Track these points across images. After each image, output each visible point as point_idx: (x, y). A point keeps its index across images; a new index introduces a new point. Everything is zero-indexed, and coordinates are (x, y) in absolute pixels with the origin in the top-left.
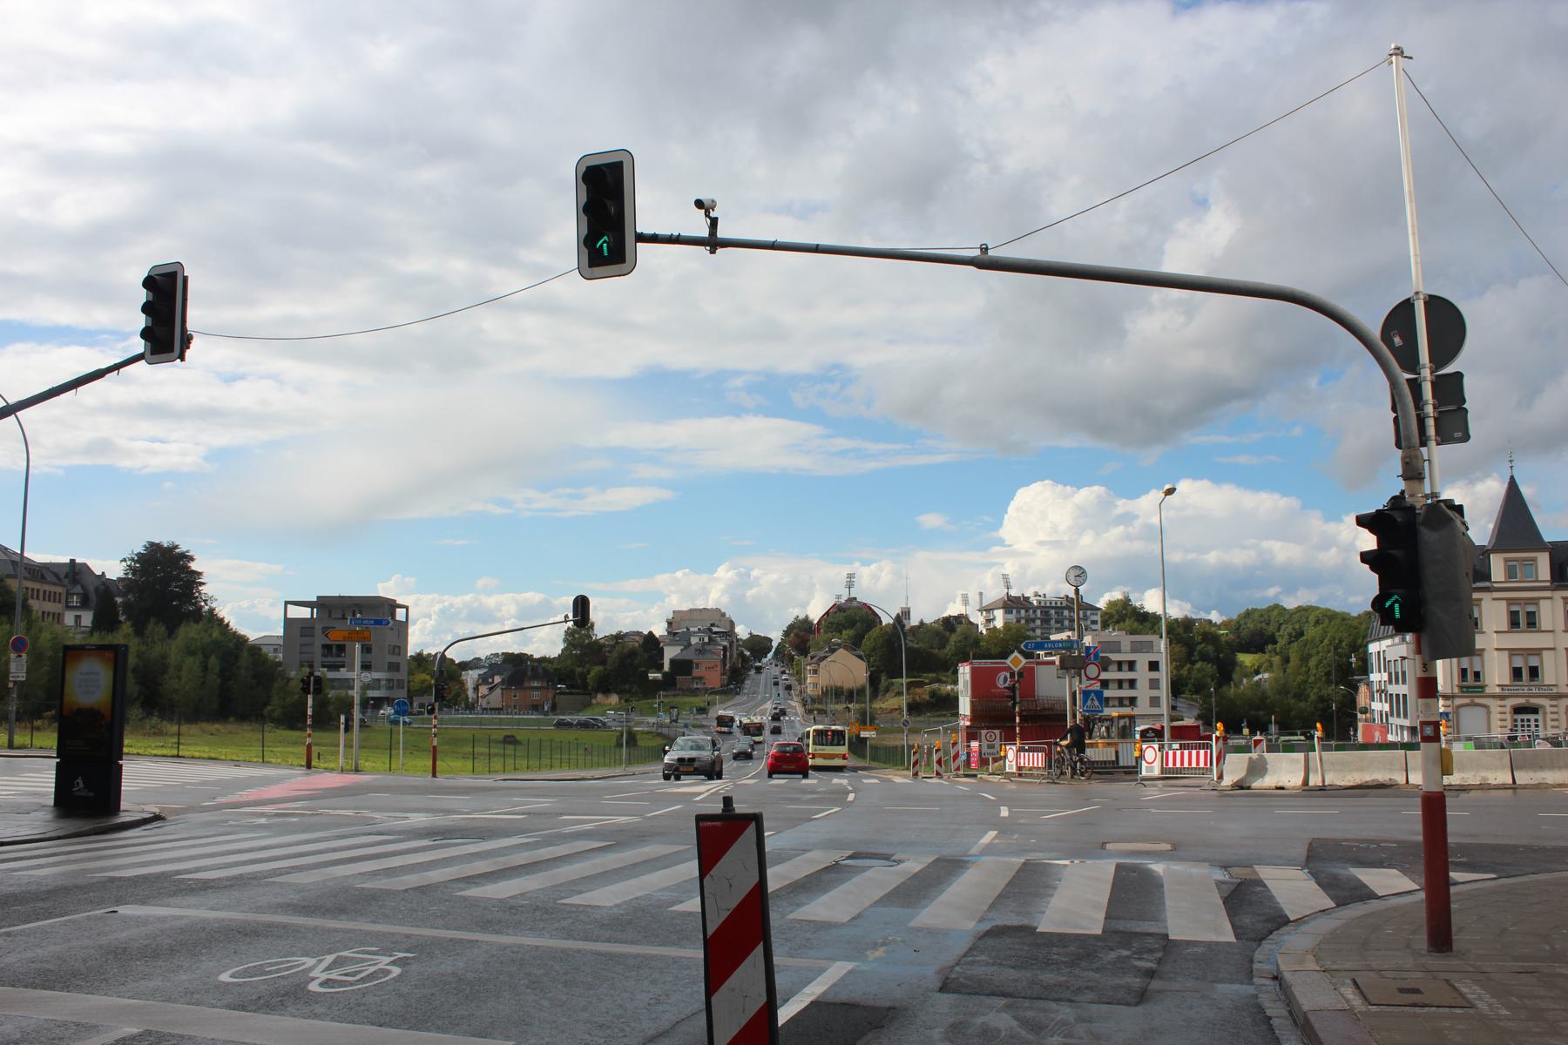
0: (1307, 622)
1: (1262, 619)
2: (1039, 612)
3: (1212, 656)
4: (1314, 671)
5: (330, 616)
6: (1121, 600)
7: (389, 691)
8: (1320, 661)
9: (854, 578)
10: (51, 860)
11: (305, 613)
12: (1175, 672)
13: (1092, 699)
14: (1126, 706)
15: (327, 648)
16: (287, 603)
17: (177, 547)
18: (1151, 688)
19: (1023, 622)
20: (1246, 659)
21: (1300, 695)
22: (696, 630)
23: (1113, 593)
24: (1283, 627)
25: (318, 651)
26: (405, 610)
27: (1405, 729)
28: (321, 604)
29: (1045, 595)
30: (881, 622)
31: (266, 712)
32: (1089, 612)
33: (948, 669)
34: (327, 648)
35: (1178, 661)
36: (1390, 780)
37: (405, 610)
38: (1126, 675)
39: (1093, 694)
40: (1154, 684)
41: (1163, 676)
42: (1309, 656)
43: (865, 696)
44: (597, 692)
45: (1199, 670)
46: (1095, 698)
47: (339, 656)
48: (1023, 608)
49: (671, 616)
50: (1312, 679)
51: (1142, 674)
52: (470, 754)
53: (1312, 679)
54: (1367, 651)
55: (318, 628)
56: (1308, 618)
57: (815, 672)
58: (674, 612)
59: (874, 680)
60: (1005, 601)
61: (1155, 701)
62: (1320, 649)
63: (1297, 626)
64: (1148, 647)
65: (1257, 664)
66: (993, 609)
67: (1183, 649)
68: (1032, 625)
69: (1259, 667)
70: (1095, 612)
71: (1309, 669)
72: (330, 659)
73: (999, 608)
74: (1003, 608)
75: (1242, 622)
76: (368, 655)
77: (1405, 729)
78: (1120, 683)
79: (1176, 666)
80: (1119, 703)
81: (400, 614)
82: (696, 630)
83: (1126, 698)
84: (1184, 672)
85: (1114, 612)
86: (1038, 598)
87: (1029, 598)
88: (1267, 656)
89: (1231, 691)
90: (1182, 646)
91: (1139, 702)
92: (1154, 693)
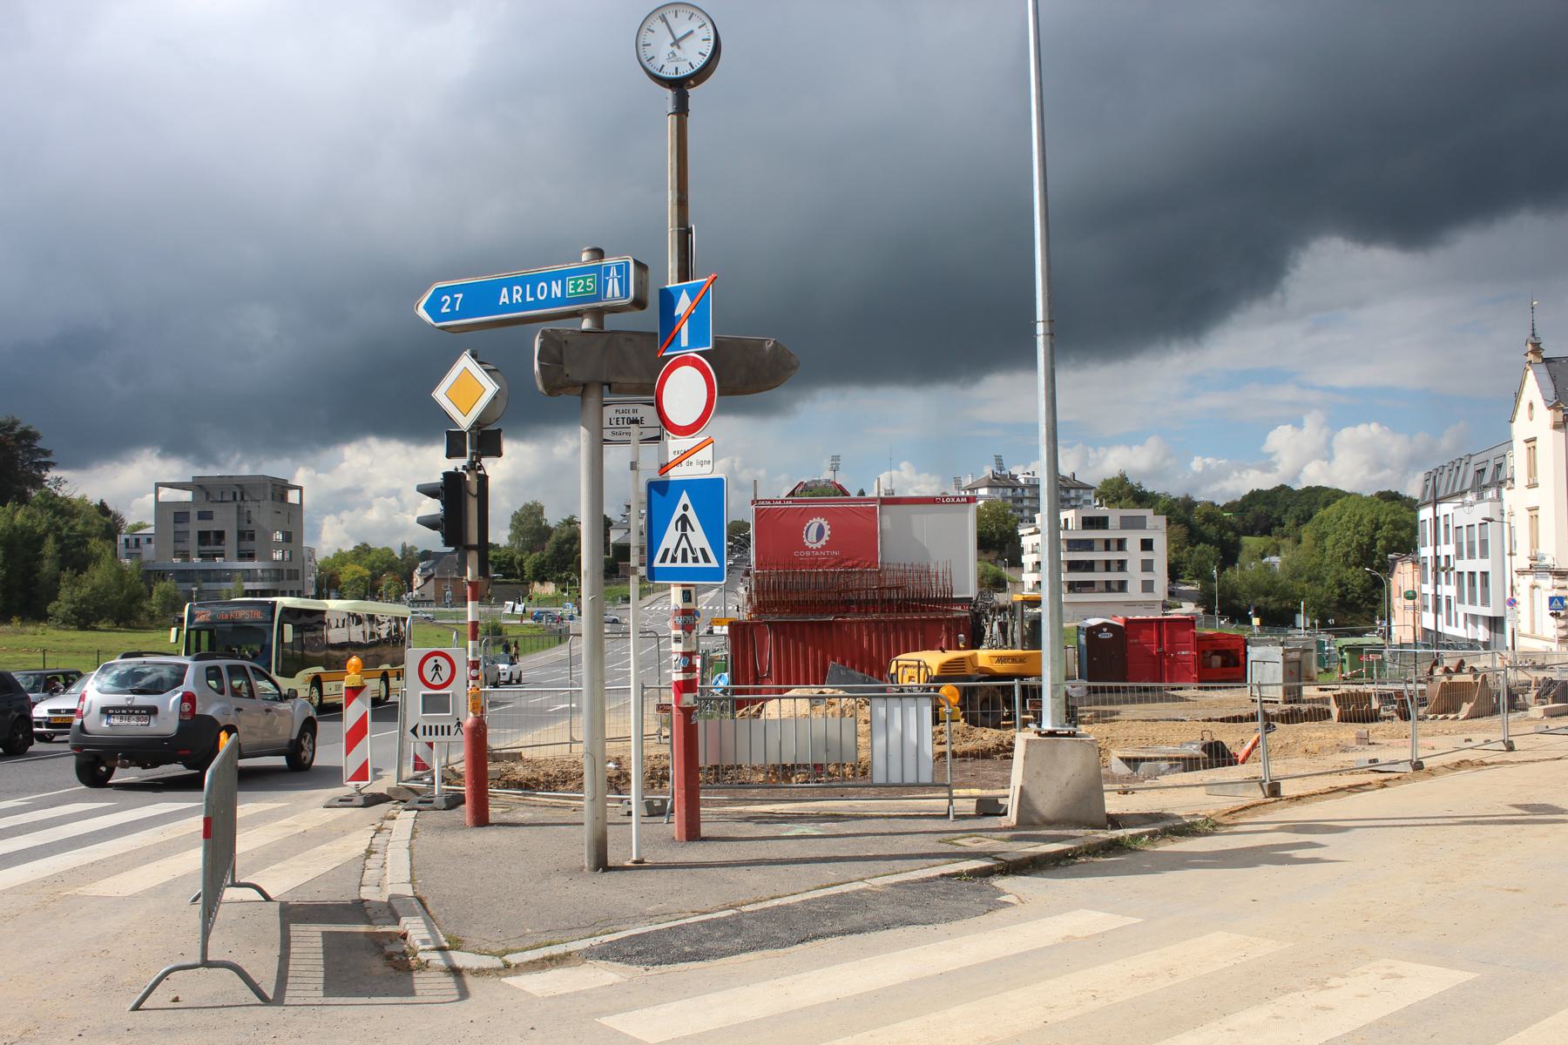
0: (1316, 503)
1: (1268, 501)
2: (1027, 490)
3: (1214, 538)
4: (1330, 552)
5: (207, 499)
6: (1117, 478)
7: (277, 583)
8: (1337, 541)
11: (186, 496)
12: (1174, 555)
13: (684, 520)
14: (1114, 591)
15: (204, 537)
16: (158, 485)
17: (15, 423)
18: (1144, 570)
19: (1010, 501)
20: (1251, 543)
21: (1316, 579)
23: (1042, 336)
24: (1290, 509)
26: (298, 491)
27: (1480, 620)
29: (1033, 473)
31: (50, 609)
32: (1081, 491)
34: (204, 537)
35: (1175, 545)
37: (298, 491)
38: (1114, 556)
39: (685, 499)
40: (1147, 566)
41: (1160, 556)
42: (1324, 535)
43: (1219, 597)
44: (533, 581)
45: (1199, 552)
46: (691, 515)
47: (218, 544)
48: (1010, 487)
50: (1327, 560)
51: (1134, 554)
53: (1327, 560)
54: (1416, 518)
55: (194, 513)
56: (1316, 499)
60: (990, 480)
61: (1148, 586)
62: (1337, 527)
63: (1306, 508)
64: (1139, 523)
65: (1262, 548)
66: (977, 488)
67: (1184, 529)
68: (1019, 505)
69: (1265, 551)
70: (1088, 491)
71: (1325, 550)
72: (207, 548)
73: (984, 487)
74: (988, 487)
75: (1246, 504)
77: (1480, 620)
78: (1108, 565)
79: (1176, 548)
80: (1119, 587)
81: (293, 497)
84: (1184, 554)
85: (1109, 492)
86: (1026, 476)
87: (1017, 476)
88: (1273, 539)
89: (1234, 575)
90: (1182, 527)
91: (1129, 587)
92: (1147, 576)
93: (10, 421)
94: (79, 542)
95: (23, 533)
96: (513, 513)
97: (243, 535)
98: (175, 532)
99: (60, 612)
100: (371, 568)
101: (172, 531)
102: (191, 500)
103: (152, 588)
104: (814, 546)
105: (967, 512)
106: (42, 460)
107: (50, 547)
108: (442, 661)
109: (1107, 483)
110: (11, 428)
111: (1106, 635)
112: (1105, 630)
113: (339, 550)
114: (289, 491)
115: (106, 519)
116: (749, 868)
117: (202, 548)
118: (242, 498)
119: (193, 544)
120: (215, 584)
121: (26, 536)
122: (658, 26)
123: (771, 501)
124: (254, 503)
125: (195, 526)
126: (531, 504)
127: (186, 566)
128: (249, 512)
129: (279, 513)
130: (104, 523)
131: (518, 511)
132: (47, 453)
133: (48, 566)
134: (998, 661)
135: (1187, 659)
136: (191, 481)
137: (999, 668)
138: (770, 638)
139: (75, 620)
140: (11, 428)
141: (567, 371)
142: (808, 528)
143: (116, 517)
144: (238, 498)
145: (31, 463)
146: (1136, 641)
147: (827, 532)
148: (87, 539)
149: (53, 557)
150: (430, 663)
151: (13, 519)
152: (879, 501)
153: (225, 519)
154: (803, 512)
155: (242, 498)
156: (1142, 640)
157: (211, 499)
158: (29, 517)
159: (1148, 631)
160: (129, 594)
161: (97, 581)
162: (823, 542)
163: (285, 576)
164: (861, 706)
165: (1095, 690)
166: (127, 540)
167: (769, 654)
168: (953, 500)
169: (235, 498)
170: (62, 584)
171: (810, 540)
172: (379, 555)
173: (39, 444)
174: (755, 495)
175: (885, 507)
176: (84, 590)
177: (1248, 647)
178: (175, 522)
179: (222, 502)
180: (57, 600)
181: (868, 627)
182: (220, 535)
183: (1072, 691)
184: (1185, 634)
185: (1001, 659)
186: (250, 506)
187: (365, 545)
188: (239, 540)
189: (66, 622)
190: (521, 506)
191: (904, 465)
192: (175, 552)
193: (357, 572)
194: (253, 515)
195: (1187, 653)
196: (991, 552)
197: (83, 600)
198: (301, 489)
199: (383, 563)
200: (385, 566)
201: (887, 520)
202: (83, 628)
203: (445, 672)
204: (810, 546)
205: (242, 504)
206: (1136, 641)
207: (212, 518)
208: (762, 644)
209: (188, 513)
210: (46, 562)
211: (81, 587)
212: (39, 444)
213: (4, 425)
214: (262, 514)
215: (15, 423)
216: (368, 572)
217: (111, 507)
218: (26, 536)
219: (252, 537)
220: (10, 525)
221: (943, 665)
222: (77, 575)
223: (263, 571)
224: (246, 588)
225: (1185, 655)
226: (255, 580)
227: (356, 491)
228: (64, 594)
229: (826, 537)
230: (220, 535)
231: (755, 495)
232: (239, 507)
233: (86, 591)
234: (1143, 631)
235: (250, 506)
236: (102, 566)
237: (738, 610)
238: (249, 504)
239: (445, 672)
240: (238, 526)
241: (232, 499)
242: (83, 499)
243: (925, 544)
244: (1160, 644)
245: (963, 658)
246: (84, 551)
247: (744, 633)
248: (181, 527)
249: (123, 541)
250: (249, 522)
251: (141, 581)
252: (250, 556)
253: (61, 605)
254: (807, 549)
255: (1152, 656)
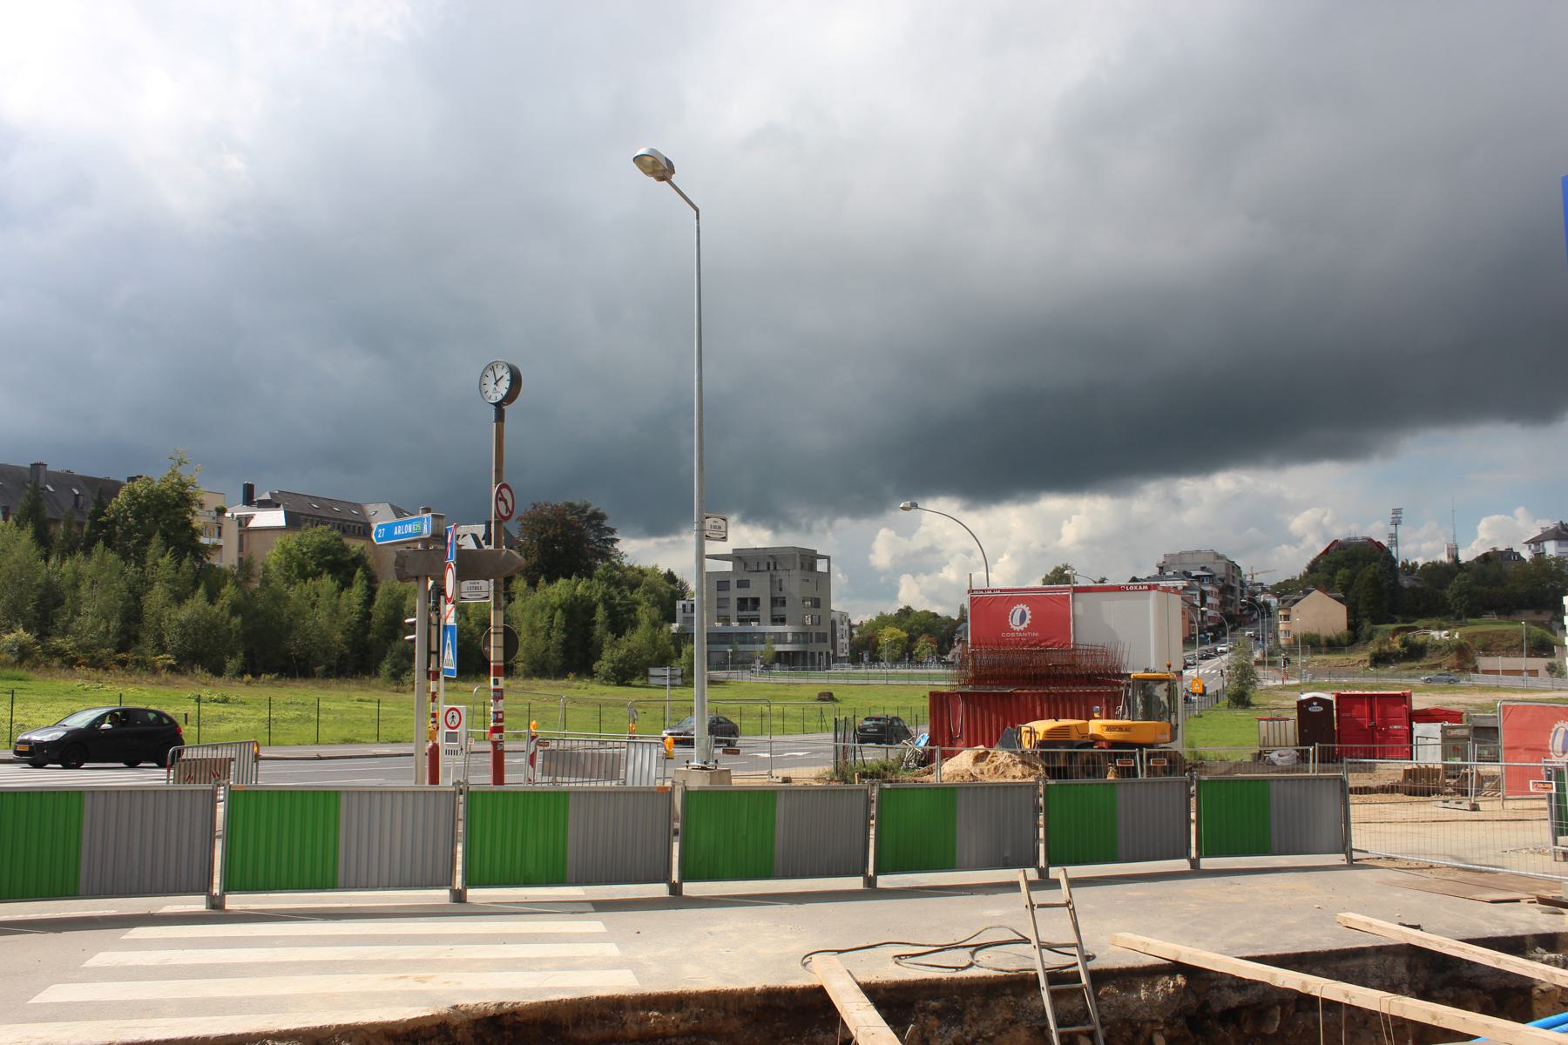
9: (1401, 513)
10: (387, 845)
11: (728, 566)
15: (742, 603)
22: (1171, 573)
25: (734, 604)
28: (739, 558)
30: (745, 520)
31: (595, 667)
33: (1227, 598)
34: (742, 603)
36: (786, 780)
47: (755, 609)
49: (1162, 560)
52: (799, 717)
55: (733, 582)
57: (1287, 617)
58: (1165, 556)
59: (1353, 626)
66: (1543, 541)
72: (745, 613)
74: (1555, 539)
76: (783, 608)
81: (821, 566)
82: (1171, 573)
83: (772, 610)
93: (583, 504)
94: (630, 609)
95: (583, 601)
96: (1044, 576)
97: (777, 601)
98: (718, 599)
99: (603, 670)
100: (909, 630)
101: (716, 598)
102: (731, 570)
103: (681, 651)
104: (1018, 628)
105: (1148, 598)
106: (608, 537)
107: (601, 614)
108: (455, 713)
109: (1313, 567)
110: (584, 511)
111: (1316, 709)
112: (1315, 704)
113: (881, 613)
114: (818, 560)
115: (672, 586)
116: (1029, 906)
117: (741, 613)
118: (775, 568)
119: (733, 610)
120: (751, 646)
121: (584, 604)
122: (490, 373)
123: (984, 591)
124: (784, 572)
125: (735, 594)
126: (1062, 567)
127: (728, 630)
128: (781, 580)
129: (808, 580)
130: (669, 590)
131: (1049, 574)
132: (612, 531)
133: (599, 630)
134: (1108, 730)
135: (1399, 733)
136: (731, 552)
137: (1109, 735)
138: (961, 706)
139: (614, 677)
140: (584, 511)
141: (407, 571)
142: (1013, 613)
143: (682, 584)
144: (772, 567)
145: (600, 540)
146: (1348, 715)
147: (1029, 617)
148: (636, 606)
149: (602, 623)
150: (450, 715)
151: (575, 590)
152: (1072, 589)
153: (760, 587)
154: (1009, 600)
155: (775, 568)
156: (1354, 714)
157: (748, 569)
158: (588, 588)
159: (1360, 706)
160: (659, 655)
161: (632, 645)
162: (1025, 625)
163: (814, 638)
164: (1014, 765)
165: (686, 734)
166: (684, 606)
167: (960, 720)
168: (1136, 588)
169: (769, 568)
170: (604, 645)
171: (1015, 623)
172: (917, 618)
173: (606, 524)
174: (971, 586)
175: (1077, 595)
176: (621, 652)
177: (1414, 723)
178: (718, 590)
179: (758, 571)
180: (601, 659)
181: (1063, 699)
182: (756, 601)
183: (1277, 760)
184: (1397, 709)
185: (1110, 728)
186: (782, 575)
187: (909, 608)
188: (772, 606)
189: (607, 679)
190: (1052, 570)
191: (1520, 511)
192: (718, 616)
193: (894, 634)
194: (784, 584)
195: (1399, 727)
196: (1545, 612)
197: (621, 660)
198: (828, 558)
199: (920, 625)
200: (923, 628)
201: (1080, 607)
202: (620, 683)
203: (457, 720)
204: (1015, 628)
205: (774, 573)
206: (1348, 715)
207: (748, 586)
208: (956, 710)
209: (729, 582)
210: (598, 627)
211: (619, 649)
212: (606, 524)
213: (578, 508)
214: (794, 585)
215: (587, 507)
216: (905, 635)
217: (678, 575)
218: (584, 604)
219: (784, 603)
220: (572, 595)
221: (1048, 732)
222: (616, 639)
223: (794, 634)
224: (777, 650)
225: (1398, 730)
226: (785, 642)
227: (932, 550)
228: (606, 655)
229: (1027, 621)
230: (756, 601)
231: (971, 586)
232: (772, 576)
233: (623, 652)
234: (1356, 706)
235: (782, 575)
236: (640, 631)
237: (1222, 675)
238: (780, 572)
239: (457, 720)
240: (771, 594)
241: (766, 568)
242: (655, 569)
243: (1112, 627)
244: (1372, 718)
245: (1068, 726)
246: (632, 616)
247: (942, 703)
248: (723, 594)
249: (681, 607)
250: (781, 590)
251: (671, 644)
252: (782, 621)
253: (603, 665)
254: (1012, 630)
255: (1363, 729)
